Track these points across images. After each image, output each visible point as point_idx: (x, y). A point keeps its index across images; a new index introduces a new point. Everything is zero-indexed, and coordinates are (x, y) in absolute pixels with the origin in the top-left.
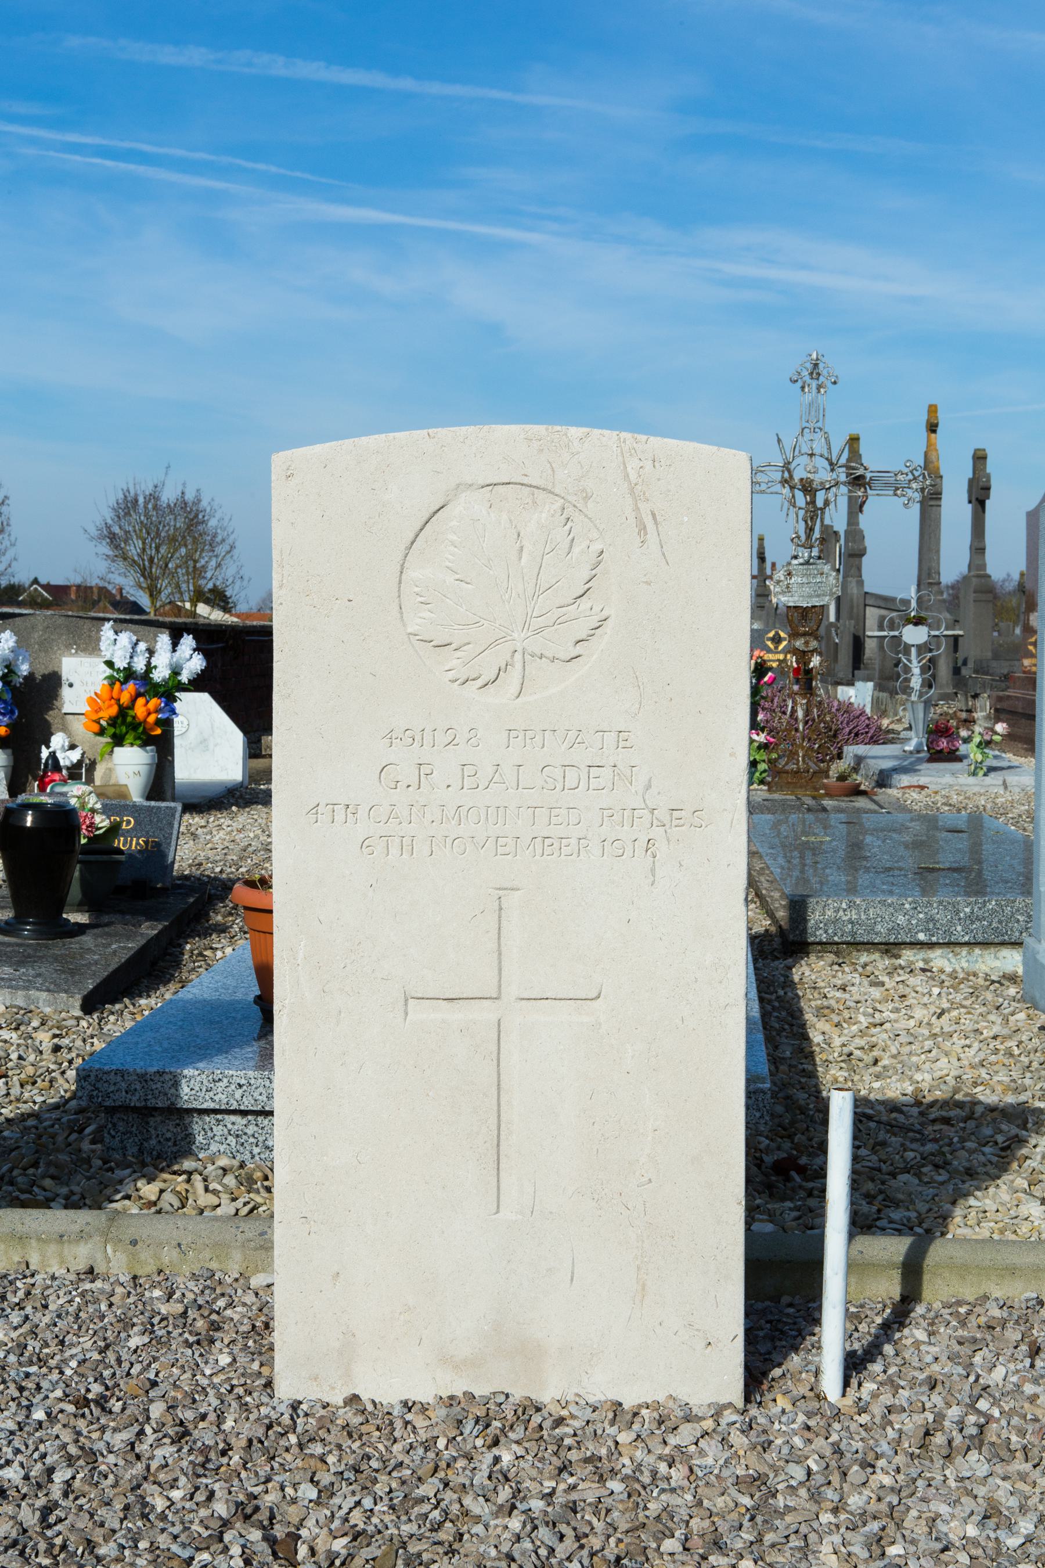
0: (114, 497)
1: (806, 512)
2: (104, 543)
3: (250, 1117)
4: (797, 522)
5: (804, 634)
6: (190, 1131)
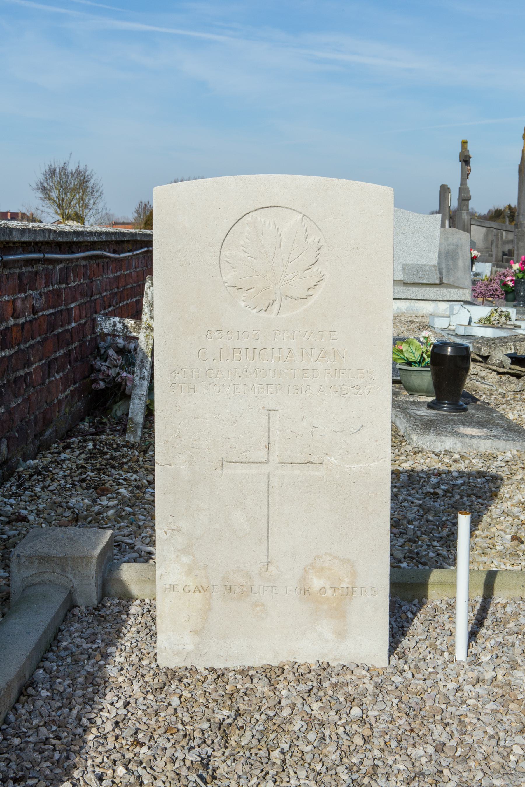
0: (45, 168)
2: (39, 192)
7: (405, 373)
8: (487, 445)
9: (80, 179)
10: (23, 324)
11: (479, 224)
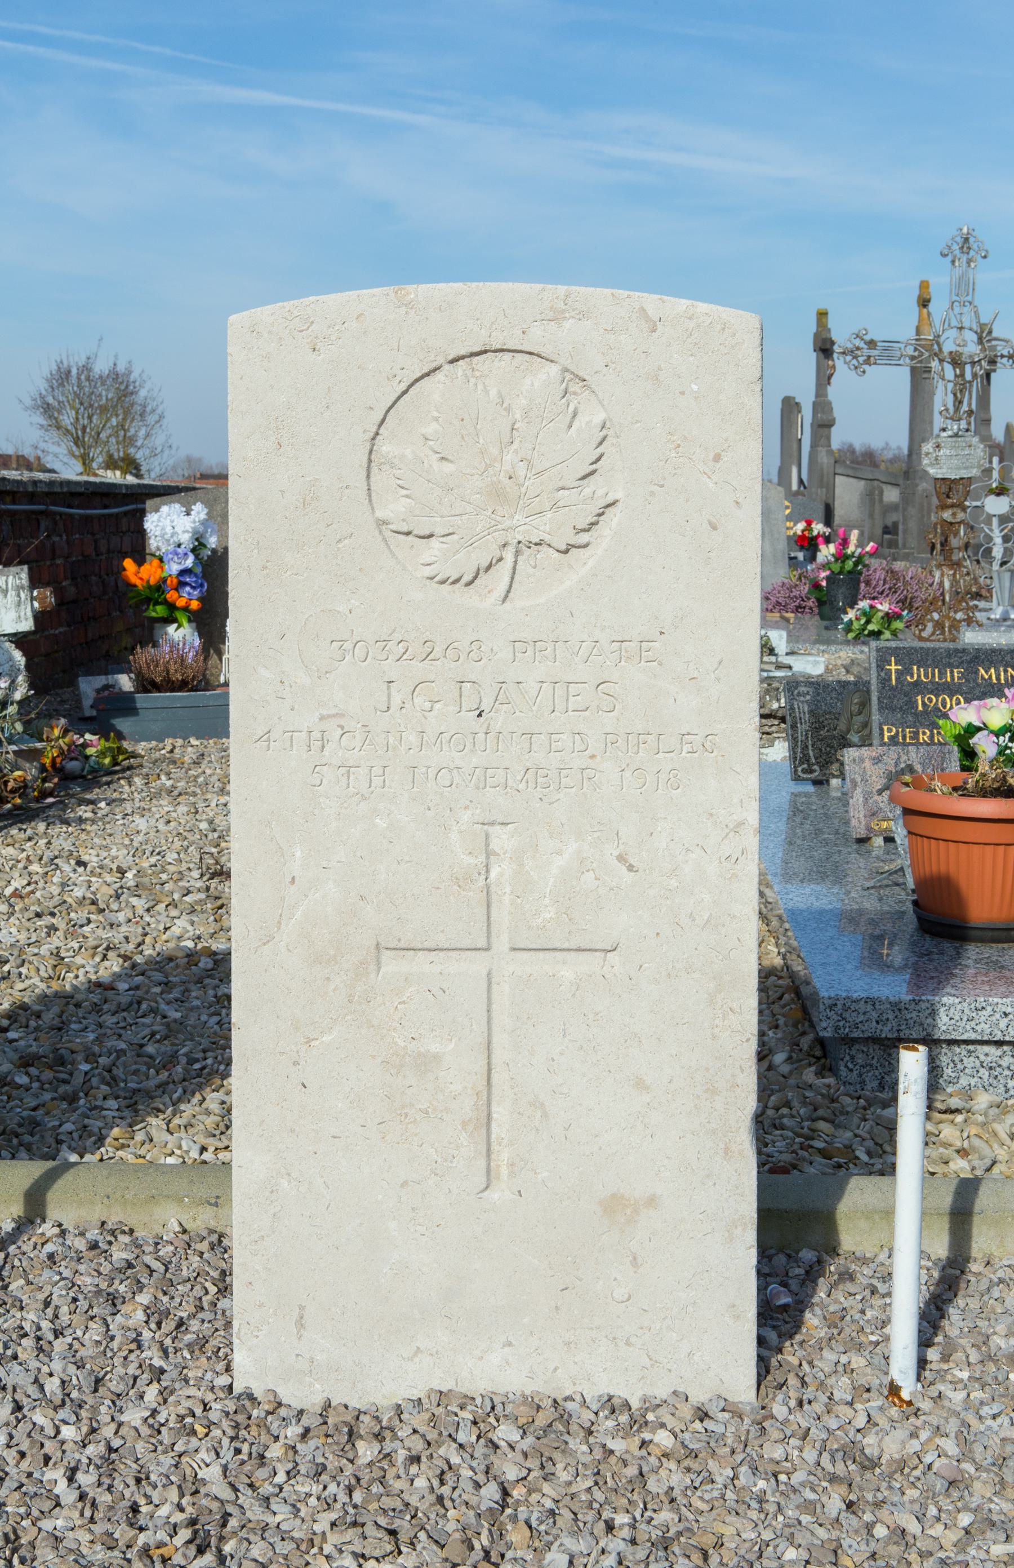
0: (49, 367)
1: (955, 385)
2: (38, 413)
3: (1005, 1048)
4: (946, 394)
5: (952, 506)
6: (938, 1063)
11: (850, 472)
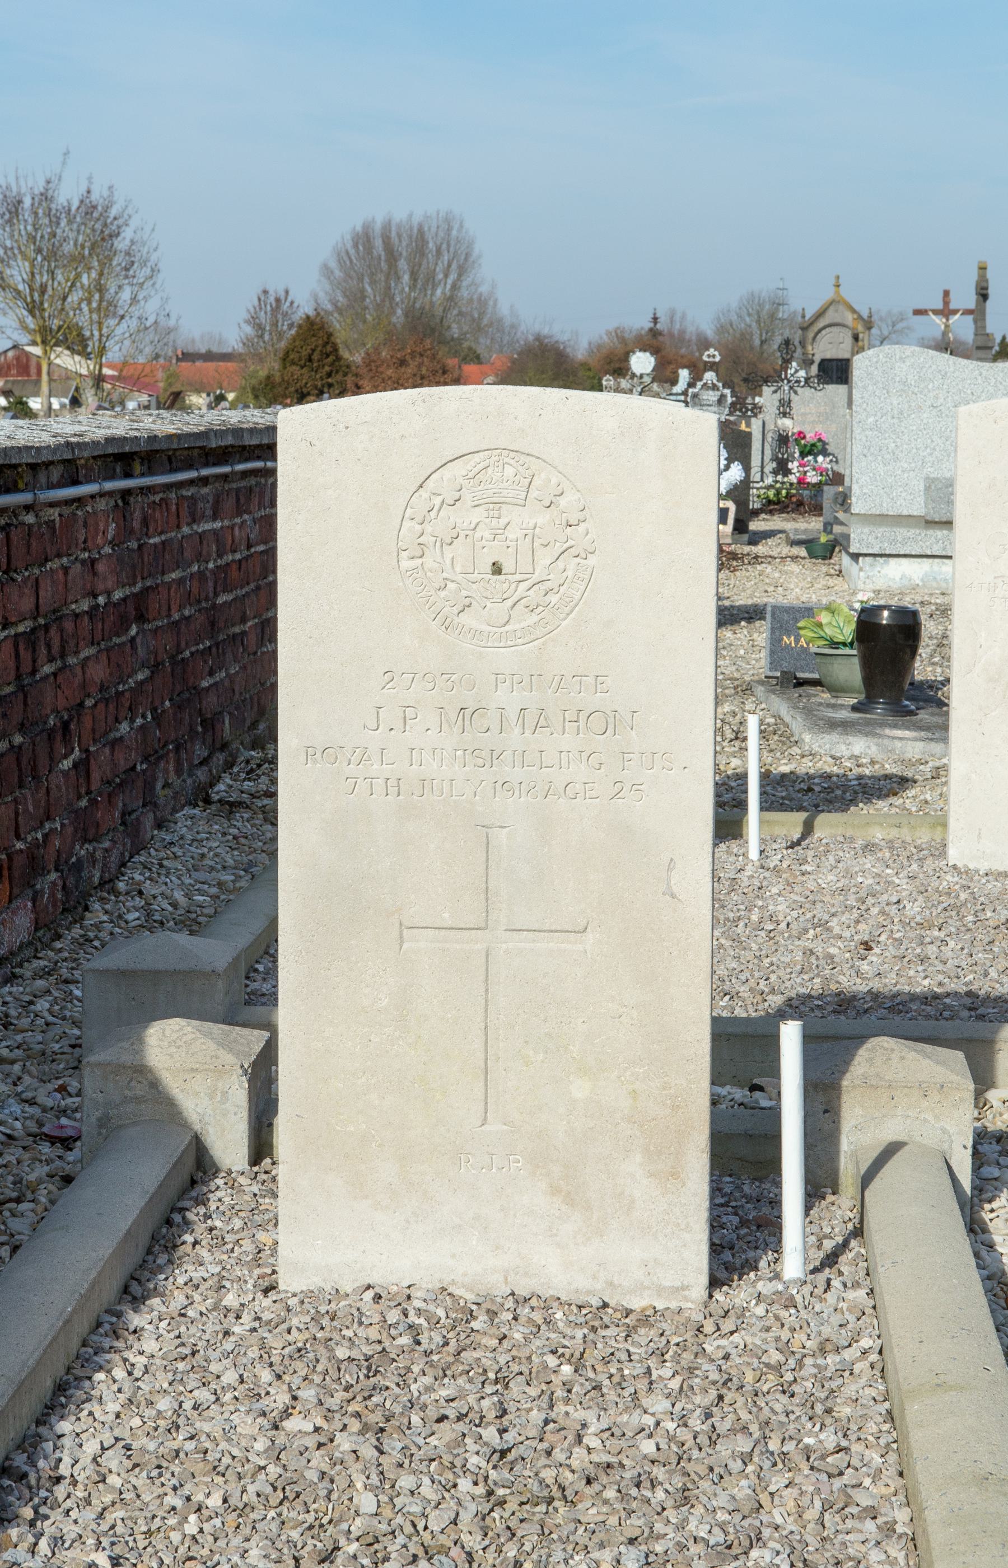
7: (824, 660)
8: (917, 750)
9: (93, 230)
10: (240, 561)
